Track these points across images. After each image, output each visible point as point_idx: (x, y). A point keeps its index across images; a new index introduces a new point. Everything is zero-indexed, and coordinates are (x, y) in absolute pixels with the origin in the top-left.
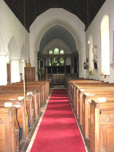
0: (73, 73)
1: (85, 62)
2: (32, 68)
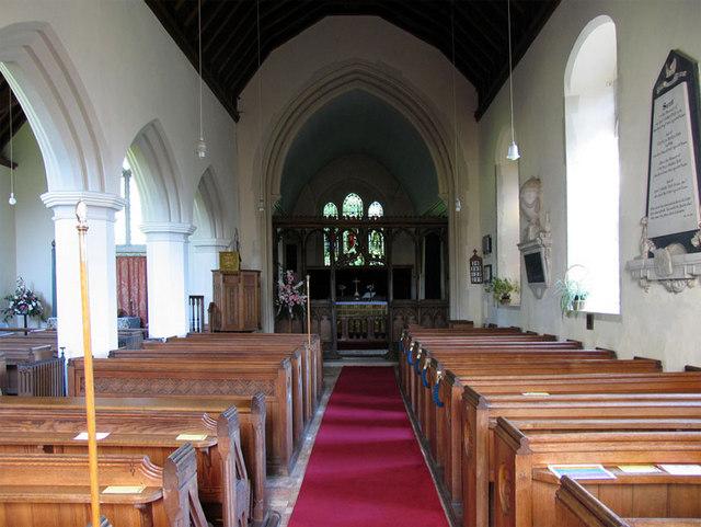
0: (422, 296)
1: (475, 251)
2: (249, 273)
